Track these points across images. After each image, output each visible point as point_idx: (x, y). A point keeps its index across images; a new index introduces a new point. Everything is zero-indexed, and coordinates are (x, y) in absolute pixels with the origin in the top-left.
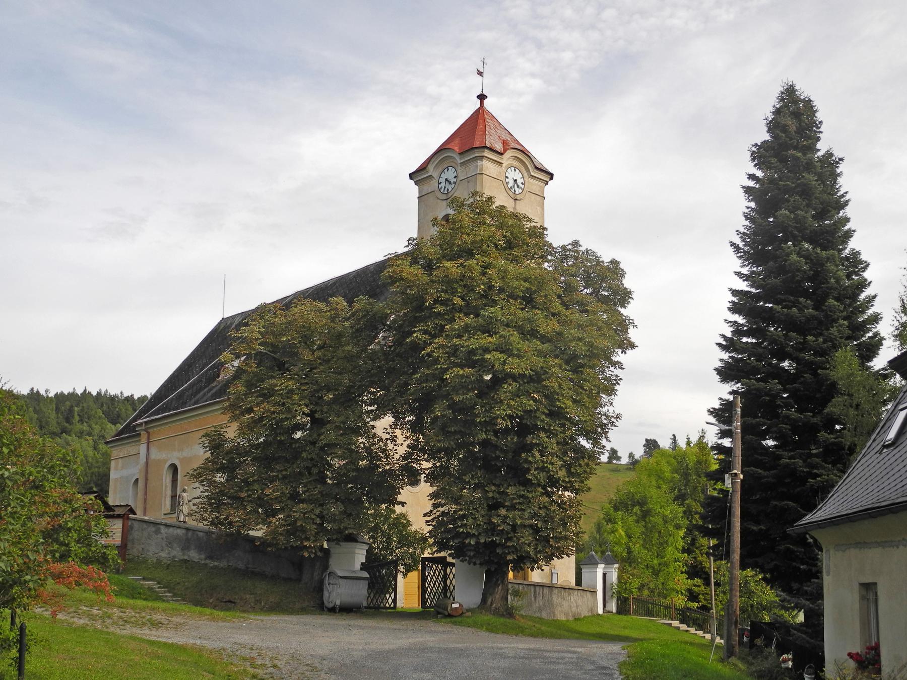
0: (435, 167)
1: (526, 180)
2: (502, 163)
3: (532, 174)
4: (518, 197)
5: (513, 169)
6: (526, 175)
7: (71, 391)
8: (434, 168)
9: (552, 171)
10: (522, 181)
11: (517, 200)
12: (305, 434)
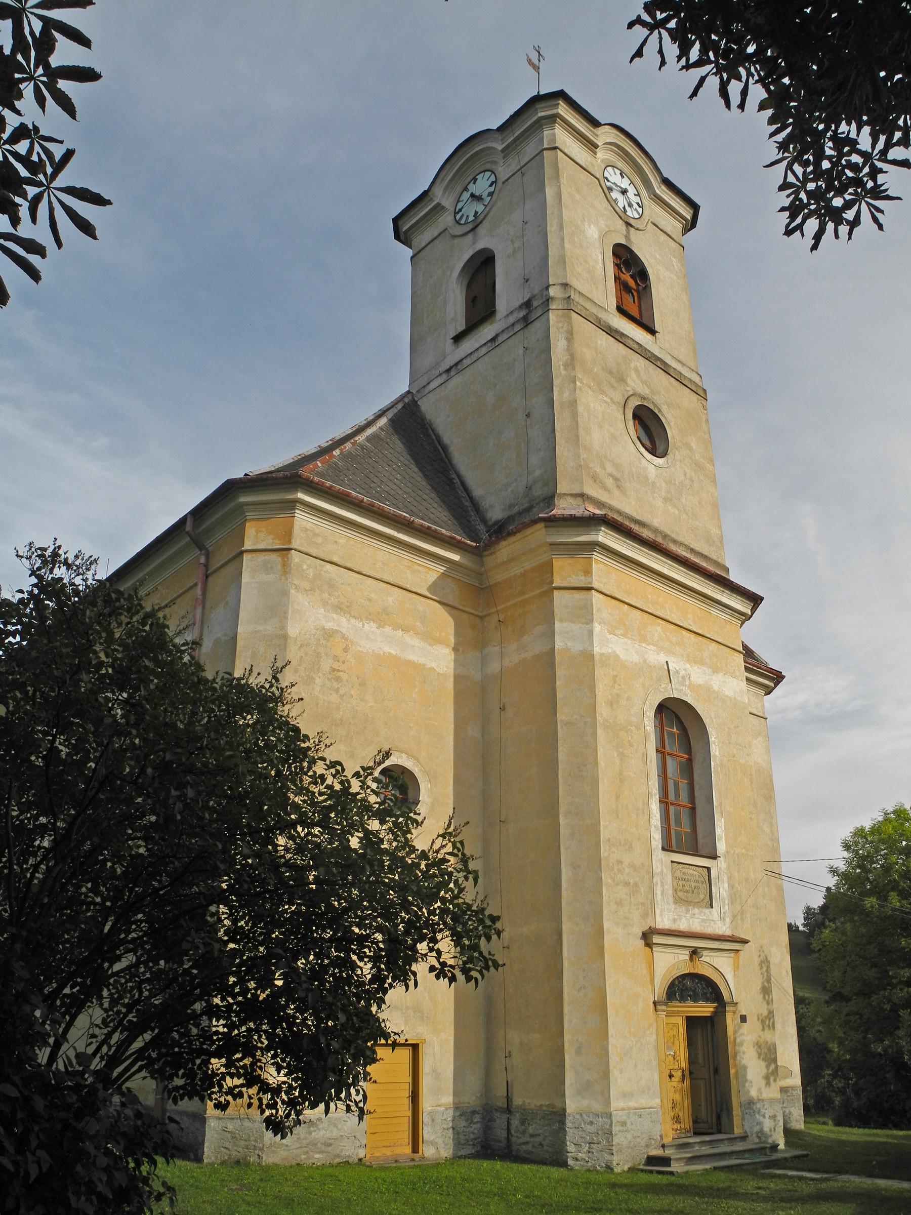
6: (644, 193)
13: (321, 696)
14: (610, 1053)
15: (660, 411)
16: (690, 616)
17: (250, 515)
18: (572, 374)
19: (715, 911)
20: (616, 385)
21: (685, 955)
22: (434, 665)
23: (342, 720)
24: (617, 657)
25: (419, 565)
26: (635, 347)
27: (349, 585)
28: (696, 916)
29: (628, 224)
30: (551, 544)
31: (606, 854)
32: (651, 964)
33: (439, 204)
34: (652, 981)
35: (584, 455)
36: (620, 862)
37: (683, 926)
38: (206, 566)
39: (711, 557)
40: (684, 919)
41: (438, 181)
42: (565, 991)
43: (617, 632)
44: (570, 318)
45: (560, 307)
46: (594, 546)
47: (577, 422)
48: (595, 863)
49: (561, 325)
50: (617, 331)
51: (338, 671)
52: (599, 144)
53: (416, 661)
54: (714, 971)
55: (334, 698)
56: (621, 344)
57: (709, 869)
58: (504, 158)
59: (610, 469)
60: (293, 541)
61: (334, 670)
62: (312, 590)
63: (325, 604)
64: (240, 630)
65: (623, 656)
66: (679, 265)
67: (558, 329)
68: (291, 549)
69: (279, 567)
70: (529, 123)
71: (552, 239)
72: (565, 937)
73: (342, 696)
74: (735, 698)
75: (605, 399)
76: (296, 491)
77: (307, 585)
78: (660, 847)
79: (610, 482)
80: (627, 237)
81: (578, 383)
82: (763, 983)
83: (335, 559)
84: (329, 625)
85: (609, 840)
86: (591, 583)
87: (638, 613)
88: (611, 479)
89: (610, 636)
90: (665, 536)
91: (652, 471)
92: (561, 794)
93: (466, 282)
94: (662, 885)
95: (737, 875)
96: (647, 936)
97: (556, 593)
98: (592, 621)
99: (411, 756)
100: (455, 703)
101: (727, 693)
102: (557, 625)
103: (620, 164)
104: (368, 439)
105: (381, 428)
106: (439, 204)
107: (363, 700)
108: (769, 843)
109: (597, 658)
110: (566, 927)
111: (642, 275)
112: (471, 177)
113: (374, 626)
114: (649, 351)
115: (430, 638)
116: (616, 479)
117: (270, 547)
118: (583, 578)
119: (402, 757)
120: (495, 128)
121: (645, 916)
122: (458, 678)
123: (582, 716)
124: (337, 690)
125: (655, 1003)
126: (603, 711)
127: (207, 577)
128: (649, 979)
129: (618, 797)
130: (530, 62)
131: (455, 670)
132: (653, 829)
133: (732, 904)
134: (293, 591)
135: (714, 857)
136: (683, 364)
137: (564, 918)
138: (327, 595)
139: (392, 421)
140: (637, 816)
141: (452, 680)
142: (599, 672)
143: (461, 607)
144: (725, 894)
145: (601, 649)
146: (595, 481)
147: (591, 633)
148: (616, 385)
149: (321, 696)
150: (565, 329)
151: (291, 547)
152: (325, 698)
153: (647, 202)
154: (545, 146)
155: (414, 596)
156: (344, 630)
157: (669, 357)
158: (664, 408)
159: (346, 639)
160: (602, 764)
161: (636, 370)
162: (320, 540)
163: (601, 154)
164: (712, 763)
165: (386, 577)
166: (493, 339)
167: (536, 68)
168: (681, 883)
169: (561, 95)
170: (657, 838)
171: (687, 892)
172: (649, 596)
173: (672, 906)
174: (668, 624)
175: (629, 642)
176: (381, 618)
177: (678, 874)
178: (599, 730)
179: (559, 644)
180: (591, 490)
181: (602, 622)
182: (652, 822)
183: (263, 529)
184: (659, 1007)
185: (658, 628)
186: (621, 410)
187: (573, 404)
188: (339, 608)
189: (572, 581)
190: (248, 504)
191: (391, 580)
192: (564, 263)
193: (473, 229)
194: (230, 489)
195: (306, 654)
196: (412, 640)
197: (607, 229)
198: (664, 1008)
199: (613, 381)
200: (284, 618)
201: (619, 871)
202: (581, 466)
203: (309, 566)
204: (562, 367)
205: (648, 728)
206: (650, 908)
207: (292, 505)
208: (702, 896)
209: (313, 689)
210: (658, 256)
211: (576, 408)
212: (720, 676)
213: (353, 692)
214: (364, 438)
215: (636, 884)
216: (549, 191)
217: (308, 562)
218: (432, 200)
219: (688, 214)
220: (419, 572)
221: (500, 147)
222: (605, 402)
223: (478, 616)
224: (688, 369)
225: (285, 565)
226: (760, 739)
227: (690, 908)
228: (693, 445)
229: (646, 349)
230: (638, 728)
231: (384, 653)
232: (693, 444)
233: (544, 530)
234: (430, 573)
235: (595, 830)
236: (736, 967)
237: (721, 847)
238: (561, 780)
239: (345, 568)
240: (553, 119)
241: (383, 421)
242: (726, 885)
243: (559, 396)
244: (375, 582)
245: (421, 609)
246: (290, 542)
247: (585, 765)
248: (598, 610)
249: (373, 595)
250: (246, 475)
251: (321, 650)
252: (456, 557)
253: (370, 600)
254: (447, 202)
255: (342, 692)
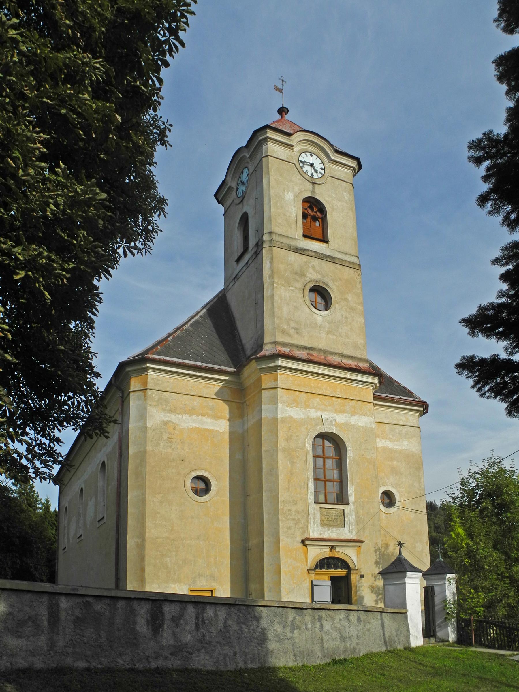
0: (233, 175)
1: (326, 165)
2: (292, 146)
3: (333, 158)
4: (317, 181)
5: (308, 154)
6: (326, 160)
7: (494, 64)
8: (232, 178)
9: (423, 399)
10: (322, 166)
11: (315, 183)
12: (457, 520)
13: (163, 450)
14: (282, 591)
15: (327, 285)
16: (338, 390)
17: (132, 375)
18: (272, 281)
19: (346, 530)
20: (299, 279)
21: (327, 549)
22: (218, 429)
23: (173, 459)
24: (291, 417)
25: (209, 384)
26: (313, 254)
27: (175, 400)
28: (334, 532)
29: (314, 183)
30: (260, 369)
31: (282, 507)
32: (306, 554)
33: (230, 186)
34: (307, 561)
35: (277, 321)
36: (290, 510)
37: (326, 536)
38: (122, 397)
39: (356, 356)
40: (326, 533)
41: (229, 174)
42: (265, 566)
43: (291, 406)
44: (272, 250)
45: (268, 246)
46: (277, 367)
47: (274, 306)
48: (276, 512)
49: (268, 255)
50: (301, 249)
51: (171, 438)
52: (293, 144)
53: (209, 428)
54: (345, 555)
55: (169, 450)
56: (304, 256)
57: (344, 510)
58: (250, 161)
59: (293, 324)
60: (148, 385)
61: (169, 438)
62: (158, 405)
63: (164, 410)
64: (130, 426)
65: (295, 417)
66: (348, 195)
67: (266, 258)
68: (147, 389)
69: (143, 397)
70: (256, 143)
71: (266, 208)
72: (265, 544)
73: (173, 449)
74: (366, 427)
75: (292, 288)
76: (146, 364)
77: (155, 403)
78: (313, 502)
79: (292, 332)
80: (313, 192)
81: (275, 285)
82: (376, 560)
83: (168, 390)
84: (166, 419)
85: (284, 501)
86: (277, 385)
87: (305, 394)
88: (293, 330)
89: (287, 408)
90: (326, 352)
91: (320, 319)
92: (263, 482)
93: (242, 229)
94: (314, 518)
95: (361, 511)
96: (303, 542)
97: (263, 391)
98: (277, 403)
99: (206, 470)
100: (229, 445)
101: (360, 425)
102: (263, 406)
103: (311, 148)
104: (191, 325)
105: (201, 317)
106: (230, 186)
107: (183, 449)
108: (418, 491)
109: (279, 420)
110: (265, 539)
111: (322, 209)
112: (241, 172)
113: (187, 416)
114: (322, 254)
115: (216, 417)
116: (296, 329)
117: (139, 389)
118: (274, 383)
119: (202, 472)
120: (244, 145)
121: (303, 533)
122: (231, 433)
123: (272, 447)
124: (171, 447)
125: (308, 570)
126: (282, 444)
127: (123, 402)
128: (305, 560)
129: (289, 482)
130: (277, 89)
131: (229, 429)
132: (309, 494)
133: (357, 525)
134: (148, 407)
135: (347, 504)
136: (346, 254)
137: (265, 536)
138: (164, 406)
139: (208, 310)
140: (300, 489)
141: (228, 434)
142: (280, 426)
143: (233, 400)
144: (353, 521)
145: (282, 415)
146: (283, 333)
147: (276, 408)
148: (299, 279)
149: (163, 450)
150: (270, 257)
151: (147, 388)
152: (165, 451)
153: (328, 165)
154: (264, 155)
155: (207, 399)
156: (173, 420)
157: (337, 252)
158: (330, 284)
159: (175, 424)
160: (280, 468)
161: (313, 267)
162: (160, 382)
163: (296, 149)
164: (348, 460)
165: (192, 393)
166: (247, 263)
167: (280, 90)
168: (326, 517)
169: (267, 127)
170: (311, 498)
171: (330, 521)
172: (312, 385)
173: (320, 528)
174: (324, 397)
175: (299, 409)
176: (191, 412)
177: (325, 513)
178: (279, 453)
179: (263, 415)
180: (280, 338)
181: (283, 402)
182: (309, 491)
183: (137, 381)
184: (310, 572)
185: (317, 400)
186: (301, 292)
187: (272, 296)
188: (171, 411)
189: (269, 385)
190: (130, 371)
191: (195, 394)
192: (271, 220)
193: (242, 201)
194: (122, 366)
195: (156, 433)
196: (206, 419)
197: (299, 191)
198: (313, 572)
199: (297, 277)
200: (145, 420)
201: (289, 514)
202: (275, 327)
203: (156, 395)
204: (268, 278)
205: (308, 448)
206: (307, 528)
207: (146, 369)
208: (339, 523)
209: (159, 448)
210: (333, 195)
211: (274, 298)
212: (356, 417)
213: (178, 446)
214: (189, 325)
215: (299, 519)
216: (265, 181)
217: (155, 393)
218: (227, 184)
219: (354, 164)
220: (210, 387)
221: (248, 156)
222: (292, 290)
223: (241, 403)
224: (349, 256)
225: (145, 396)
226: (414, 439)
227: (331, 528)
228: (349, 298)
229: (320, 253)
230: (302, 449)
231: (193, 427)
232: (349, 298)
233: (255, 363)
234: (215, 387)
235: (276, 498)
236: (359, 553)
237: (351, 499)
238: (263, 476)
239: (173, 393)
240: (266, 140)
241: (204, 310)
242: (354, 517)
243: (266, 293)
244: (188, 396)
245: (211, 404)
246: (147, 386)
247: (273, 469)
248: (281, 397)
249: (187, 402)
250: (128, 358)
251: (162, 430)
252: (226, 378)
253: (185, 405)
254: (234, 185)
255: (173, 447)
